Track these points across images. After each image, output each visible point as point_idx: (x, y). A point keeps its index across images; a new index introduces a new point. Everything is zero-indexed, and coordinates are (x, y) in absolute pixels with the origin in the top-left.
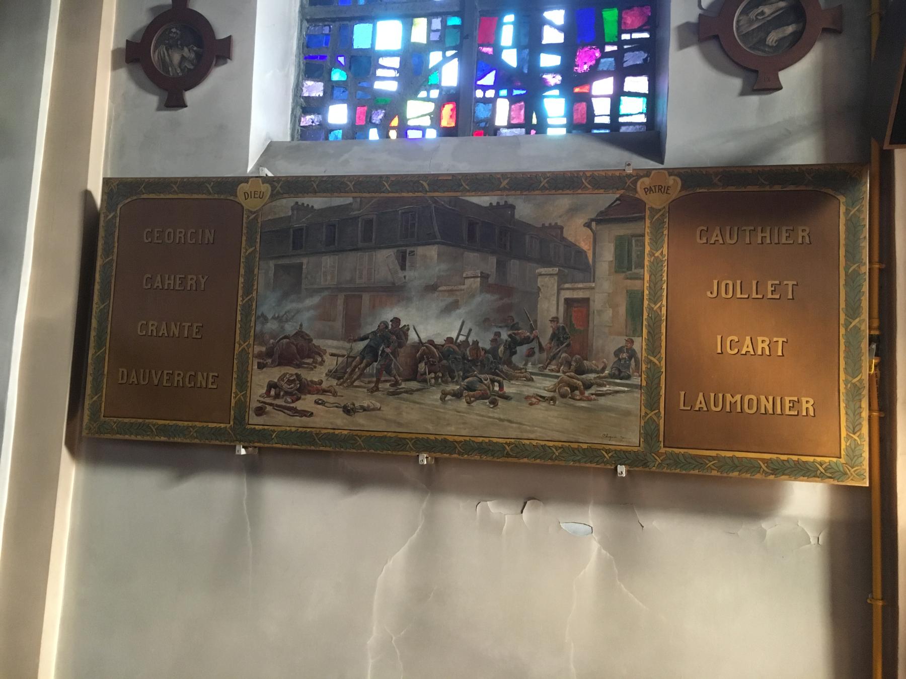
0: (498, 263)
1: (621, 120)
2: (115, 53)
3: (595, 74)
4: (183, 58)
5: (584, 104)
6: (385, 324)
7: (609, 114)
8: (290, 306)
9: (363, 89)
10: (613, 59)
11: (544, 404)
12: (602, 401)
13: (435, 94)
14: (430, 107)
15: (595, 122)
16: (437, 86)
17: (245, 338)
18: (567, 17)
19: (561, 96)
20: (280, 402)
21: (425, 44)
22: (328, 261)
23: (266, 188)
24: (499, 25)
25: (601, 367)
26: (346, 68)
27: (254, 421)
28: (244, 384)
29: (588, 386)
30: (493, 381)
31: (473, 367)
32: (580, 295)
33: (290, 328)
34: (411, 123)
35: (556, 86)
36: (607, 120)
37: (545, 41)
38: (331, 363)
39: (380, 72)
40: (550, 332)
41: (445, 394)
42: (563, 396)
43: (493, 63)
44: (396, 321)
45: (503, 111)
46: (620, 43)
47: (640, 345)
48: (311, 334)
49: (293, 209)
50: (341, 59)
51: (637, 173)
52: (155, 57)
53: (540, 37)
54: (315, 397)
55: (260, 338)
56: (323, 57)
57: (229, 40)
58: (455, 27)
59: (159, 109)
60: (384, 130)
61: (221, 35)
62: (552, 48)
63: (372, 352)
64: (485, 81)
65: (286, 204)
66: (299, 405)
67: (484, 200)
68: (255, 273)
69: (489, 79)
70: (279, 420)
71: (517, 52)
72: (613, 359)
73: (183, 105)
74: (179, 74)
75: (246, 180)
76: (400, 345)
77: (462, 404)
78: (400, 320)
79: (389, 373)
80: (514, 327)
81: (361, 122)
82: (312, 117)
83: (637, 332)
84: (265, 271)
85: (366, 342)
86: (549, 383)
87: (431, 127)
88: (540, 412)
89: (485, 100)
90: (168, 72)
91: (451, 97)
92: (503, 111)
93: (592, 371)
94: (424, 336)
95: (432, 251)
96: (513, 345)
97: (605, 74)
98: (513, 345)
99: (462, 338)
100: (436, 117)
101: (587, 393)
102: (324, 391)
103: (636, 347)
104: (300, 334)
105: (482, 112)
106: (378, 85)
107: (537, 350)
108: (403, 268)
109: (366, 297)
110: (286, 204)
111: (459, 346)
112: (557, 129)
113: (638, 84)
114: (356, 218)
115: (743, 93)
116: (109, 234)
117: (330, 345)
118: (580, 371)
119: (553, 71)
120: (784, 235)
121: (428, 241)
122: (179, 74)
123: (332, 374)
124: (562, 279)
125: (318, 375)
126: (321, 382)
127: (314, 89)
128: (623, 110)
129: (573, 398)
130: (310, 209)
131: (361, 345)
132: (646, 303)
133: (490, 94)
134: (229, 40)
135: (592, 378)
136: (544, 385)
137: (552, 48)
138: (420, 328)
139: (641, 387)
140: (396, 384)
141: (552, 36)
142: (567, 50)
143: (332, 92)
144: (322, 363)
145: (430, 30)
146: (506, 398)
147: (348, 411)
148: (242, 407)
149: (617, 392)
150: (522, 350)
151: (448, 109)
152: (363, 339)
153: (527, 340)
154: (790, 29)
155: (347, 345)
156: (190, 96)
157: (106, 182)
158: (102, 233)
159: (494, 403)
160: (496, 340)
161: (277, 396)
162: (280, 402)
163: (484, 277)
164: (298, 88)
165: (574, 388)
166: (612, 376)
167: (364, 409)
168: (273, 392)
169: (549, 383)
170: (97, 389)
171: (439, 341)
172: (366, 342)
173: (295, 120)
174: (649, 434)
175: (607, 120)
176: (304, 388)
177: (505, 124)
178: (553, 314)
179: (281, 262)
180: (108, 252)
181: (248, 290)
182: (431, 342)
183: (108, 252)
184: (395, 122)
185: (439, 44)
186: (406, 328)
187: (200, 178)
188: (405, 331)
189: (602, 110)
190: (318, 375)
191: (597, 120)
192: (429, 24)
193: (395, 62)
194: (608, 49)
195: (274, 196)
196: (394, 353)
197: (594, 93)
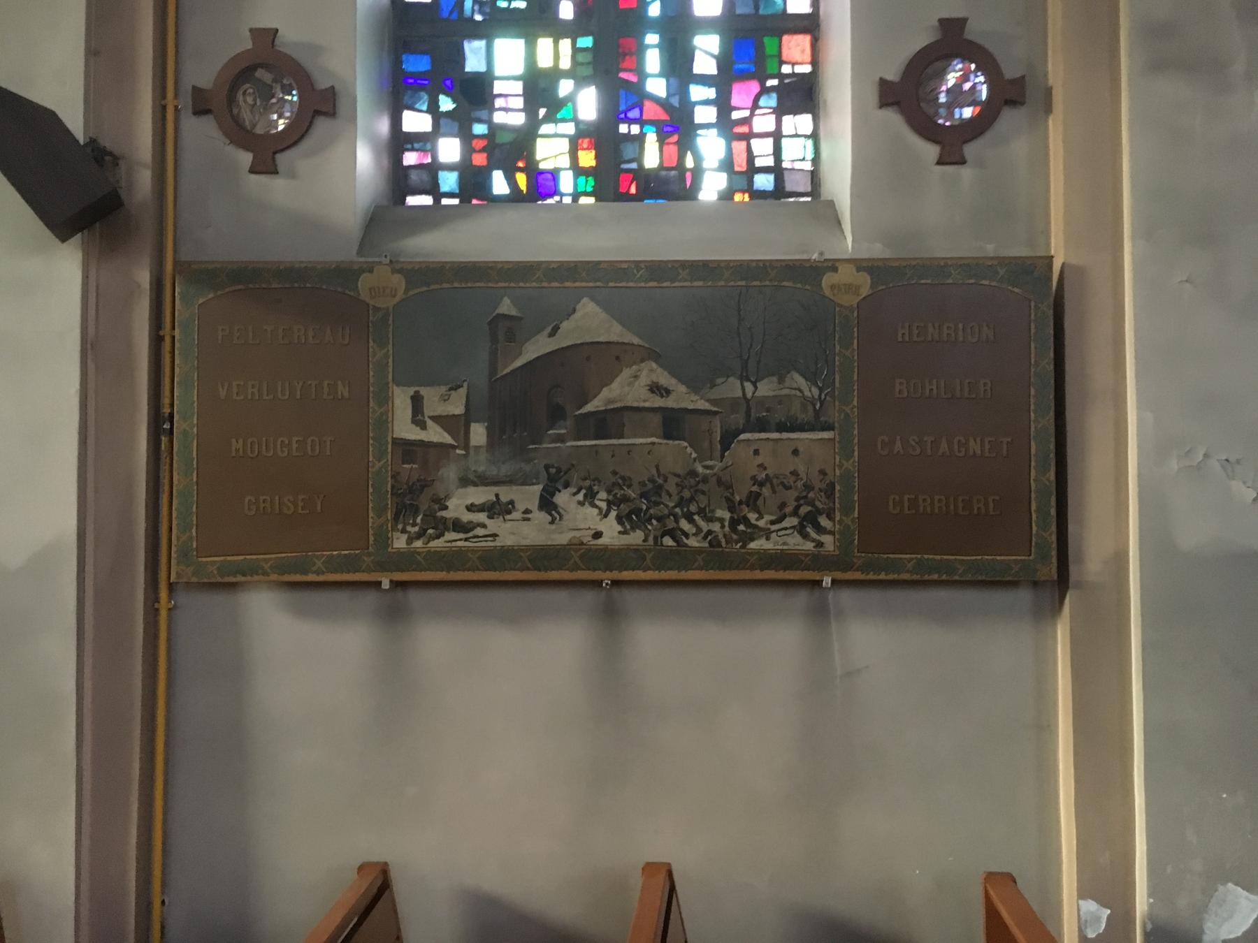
10: (621, 7)
13: (570, 128)
15: (467, 69)
18: (723, 44)
24: (641, 49)
36: (770, 162)
39: (499, 103)
51: (554, 175)
62: (704, 80)
71: (782, 131)
74: (275, 117)
113: (802, 123)
115: (940, 162)
120: (311, 334)
122: (275, 117)
137: (704, 80)
141: (705, 64)
142: (724, 80)
175: (770, 162)
187: (1004, 257)
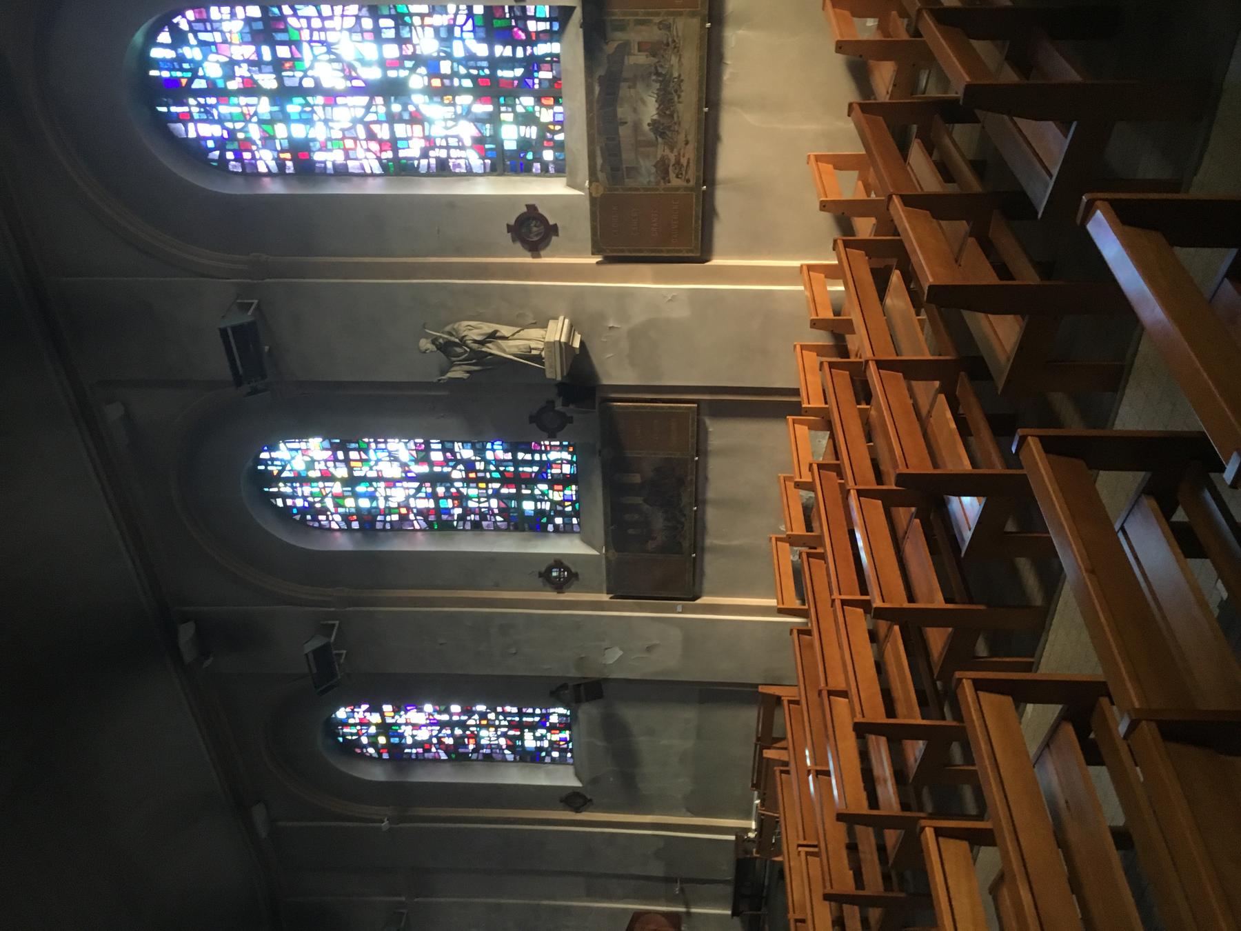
0: (624, 81)
1: (548, 16)
2: (533, 257)
3: (525, 30)
4: (535, 226)
5: (541, 35)
6: (650, 129)
8: (643, 171)
9: (536, 143)
11: (682, 59)
12: (680, 34)
13: (537, 108)
14: (544, 110)
16: (533, 107)
17: (658, 190)
19: (536, 46)
20: (684, 173)
21: (860, 172)
22: (624, 156)
23: (594, 184)
25: (666, 36)
26: (526, 152)
27: (692, 183)
28: (677, 189)
29: (674, 41)
30: (673, 82)
31: (693, 910)
32: (636, 47)
33: (653, 170)
34: (552, 120)
35: (532, 49)
36: (548, 23)
37: (511, 55)
38: (667, 152)
39: (528, 136)
40: (652, 58)
41: (679, 102)
42: (678, 51)
43: (522, 79)
44: (649, 125)
45: (546, 75)
46: (511, 18)
47: (657, 20)
48: (655, 161)
49: (602, 172)
50: (522, 155)
52: (535, 239)
53: (509, 58)
54: (681, 157)
55: (658, 183)
56: (521, 164)
57: (527, 206)
58: (505, 100)
59: (557, 235)
60: (554, 132)
61: (525, 210)
62: (514, 51)
63: (662, 135)
64: (531, 84)
65: (601, 176)
66: (685, 164)
67: (597, 89)
68: (466, 376)
69: (530, 82)
70: (692, 174)
72: (663, 31)
73: (556, 225)
75: (591, 194)
76: (659, 122)
77: (683, 94)
79: (671, 126)
80: (650, 74)
81: (552, 144)
82: (550, 168)
83: (650, 21)
84: (629, 183)
85: (658, 137)
86: (673, 58)
87: (553, 109)
88: (685, 61)
89: (540, 83)
90: (541, 233)
91: (538, 101)
92: (546, 75)
93: (668, 39)
94: (655, 112)
95: (619, 110)
96: (658, 74)
97: (526, 25)
98: (658, 74)
99: (655, 96)
100: (549, 107)
101: (677, 41)
102: (679, 154)
103: (658, 21)
104: (655, 166)
105: (546, 85)
106: (534, 137)
107: (660, 63)
108: (626, 123)
109: (639, 138)
110: (601, 176)
111: (658, 96)
112: (555, 48)
114: (606, 145)
116: (615, 251)
117: (660, 153)
118: (668, 45)
119: (525, 50)
121: (615, 115)
123: (672, 150)
124: (630, 54)
125: (672, 157)
126: (675, 156)
127: (537, 167)
128: (543, 16)
129: (679, 47)
130: (602, 166)
131: (660, 140)
132: (639, 18)
133: (536, 81)
134: (527, 206)
136: (674, 60)
137: (514, 51)
138: (652, 114)
139: (674, 19)
140: (675, 123)
143: (538, 158)
144: (667, 155)
145: (507, 112)
146: (680, 76)
147: (687, 143)
148: (686, 189)
150: (660, 70)
151: (544, 101)
152: (657, 139)
153: (656, 68)
155: (659, 146)
156: (551, 222)
157: (593, 254)
158: (615, 254)
159: (682, 81)
160: (656, 81)
161: (682, 174)
162: (684, 173)
163: (629, 87)
164: (536, 175)
165: (675, 47)
166: (670, 31)
167: (686, 136)
168: (680, 176)
169: (673, 58)
170: (680, 251)
171: (657, 105)
172: (658, 137)
173: (551, 176)
174: (693, 15)
175: (548, 23)
176: (678, 163)
177: (551, 73)
178: (645, 57)
179: (625, 176)
180: (623, 251)
181: (637, 189)
182: (658, 109)
183: (623, 251)
184: (551, 127)
185: (513, 106)
186: (653, 120)
188: (654, 121)
190: (672, 157)
192: (504, 112)
193: (522, 128)
194: (513, 24)
195: (597, 180)
196: (663, 124)
197: (535, 30)
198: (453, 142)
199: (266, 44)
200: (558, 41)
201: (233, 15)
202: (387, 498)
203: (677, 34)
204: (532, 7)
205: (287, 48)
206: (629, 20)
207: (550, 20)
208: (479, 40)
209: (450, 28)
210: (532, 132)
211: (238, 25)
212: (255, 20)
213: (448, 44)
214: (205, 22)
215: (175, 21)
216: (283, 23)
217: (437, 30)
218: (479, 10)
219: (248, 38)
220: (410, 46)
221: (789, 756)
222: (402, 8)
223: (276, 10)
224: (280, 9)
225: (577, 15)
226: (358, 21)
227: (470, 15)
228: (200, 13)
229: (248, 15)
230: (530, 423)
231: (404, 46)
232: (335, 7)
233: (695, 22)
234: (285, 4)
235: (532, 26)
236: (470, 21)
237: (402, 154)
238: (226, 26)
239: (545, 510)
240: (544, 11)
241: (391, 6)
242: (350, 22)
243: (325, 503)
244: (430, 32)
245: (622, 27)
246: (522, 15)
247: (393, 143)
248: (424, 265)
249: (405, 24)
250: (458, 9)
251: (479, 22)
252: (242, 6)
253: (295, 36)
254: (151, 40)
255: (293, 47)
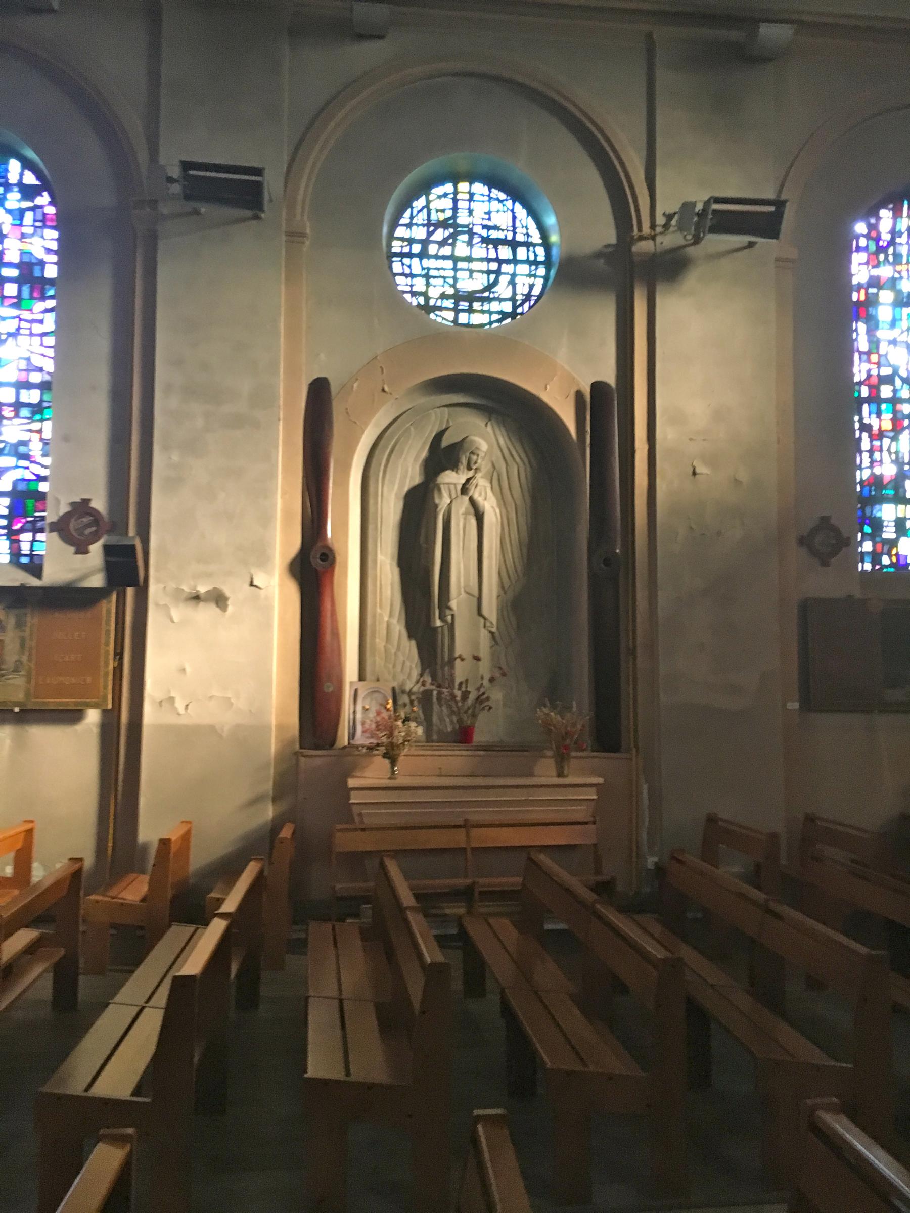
1: (34, 553)
3: (22, 530)
7: (443, 229)
12: (9, 681)
47: (25, 658)
78: (592, 384)
135: (547, 709)
149: (15, 678)
154: (94, 529)
174: (27, 694)
175: (28, 553)
180: (108, 632)
189: (25, 548)
191: (23, 552)
198: (877, 456)
199: (21, 275)
200: (10, 561)
201: (49, 251)
202: (894, 342)
203: (9, 679)
204: (44, 539)
205: (15, 293)
206: (24, 631)
207: (31, 556)
208: (15, 483)
209: (26, 457)
210: (889, 533)
211: (40, 254)
212: (43, 270)
213: (13, 453)
214: (43, 222)
215: (45, 194)
216: (38, 296)
217: (25, 443)
218: (43, 487)
219: (26, 259)
220: (12, 414)
221: (192, 927)
222: (48, 414)
223: (51, 292)
224: (52, 297)
225: (34, 582)
226: (38, 369)
227: (40, 478)
228: (52, 220)
229: (47, 265)
230: (825, 520)
231: (12, 409)
232: (52, 350)
233: (20, 696)
234: (57, 303)
235: (26, 537)
236: (34, 477)
237: (865, 407)
238: (36, 240)
239: (882, 531)
240: (40, 549)
241: (51, 404)
242: (37, 361)
243: (884, 265)
244: (25, 436)
245: (19, 625)
246: (37, 528)
247: (874, 399)
248: (585, 413)
249: (34, 413)
250: (46, 467)
251: (32, 486)
252: (545, 276)
253: (25, 304)
254: (27, 164)
255: (15, 300)
